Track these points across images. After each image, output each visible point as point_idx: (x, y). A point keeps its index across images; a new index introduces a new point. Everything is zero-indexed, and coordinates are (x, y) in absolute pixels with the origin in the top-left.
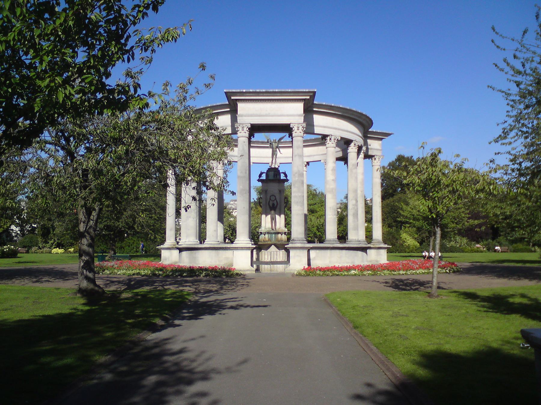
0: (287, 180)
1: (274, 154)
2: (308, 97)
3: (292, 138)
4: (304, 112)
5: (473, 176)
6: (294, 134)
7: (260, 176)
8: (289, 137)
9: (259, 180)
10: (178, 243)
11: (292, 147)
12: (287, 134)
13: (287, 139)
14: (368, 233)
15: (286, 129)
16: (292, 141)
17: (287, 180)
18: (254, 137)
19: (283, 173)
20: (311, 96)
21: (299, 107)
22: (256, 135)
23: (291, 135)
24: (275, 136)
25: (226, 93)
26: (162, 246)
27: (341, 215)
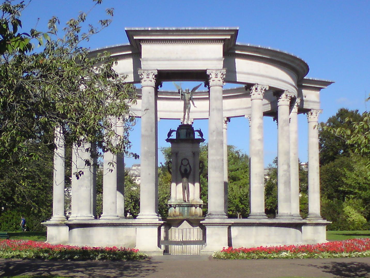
0: (203, 140)
1: (186, 107)
3: (209, 88)
7: (169, 135)
9: (168, 140)
12: (203, 83)
13: (203, 88)
15: (202, 76)
17: (203, 140)
20: (232, 36)
22: (164, 84)
23: (207, 84)
24: (187, 85)
26: (48, 222)
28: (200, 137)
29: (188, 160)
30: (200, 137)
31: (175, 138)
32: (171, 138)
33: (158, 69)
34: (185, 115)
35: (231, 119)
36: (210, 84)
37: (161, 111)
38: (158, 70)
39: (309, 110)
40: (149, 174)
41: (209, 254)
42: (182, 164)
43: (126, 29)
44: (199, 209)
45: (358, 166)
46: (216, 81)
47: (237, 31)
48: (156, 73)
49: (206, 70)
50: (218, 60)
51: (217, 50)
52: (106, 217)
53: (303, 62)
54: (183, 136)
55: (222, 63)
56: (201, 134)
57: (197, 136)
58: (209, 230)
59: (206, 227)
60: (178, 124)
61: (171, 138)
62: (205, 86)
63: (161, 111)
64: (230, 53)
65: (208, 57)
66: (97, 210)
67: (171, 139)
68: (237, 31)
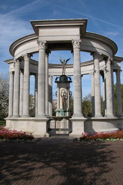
0: (71, 82)
6: (74, 50)
7: (56, 79)
9: (55, 82)
18: (50, 53)
20: (84, 23)
34: (63, 71)
35: (83, 75)
40: (42, 94)
41: (75, 137)
43: (31, 21)
44: (38, 59)
45: (34, 159)
46: (76, 47)
49: (71, 41)
50: (77, 35)
51: (76, 31)
54: (62, 80)
56: (71, 79)
57: (69, 80)
58: (74, 123)
59: (72, 122)
62: (72, 53)
64: (83, 35)
65: (72, 34)
68: (87, 20)
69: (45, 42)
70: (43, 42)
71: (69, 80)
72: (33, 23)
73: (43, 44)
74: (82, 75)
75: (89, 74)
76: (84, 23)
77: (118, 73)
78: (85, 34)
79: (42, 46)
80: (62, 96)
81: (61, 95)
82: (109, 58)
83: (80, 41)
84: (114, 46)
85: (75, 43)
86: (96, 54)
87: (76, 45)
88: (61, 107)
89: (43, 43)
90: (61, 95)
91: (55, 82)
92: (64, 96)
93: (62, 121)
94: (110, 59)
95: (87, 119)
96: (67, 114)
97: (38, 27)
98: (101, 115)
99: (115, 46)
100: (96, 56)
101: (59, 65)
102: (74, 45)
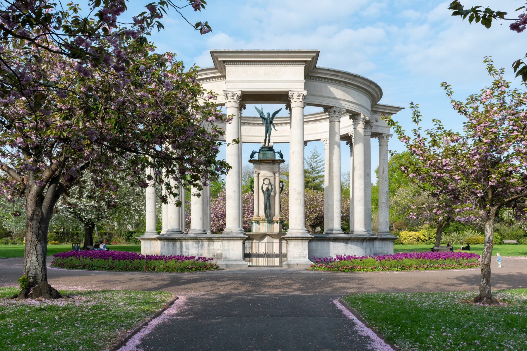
0: (283, 161)
1: (268, 131)
2: (310, 59)
3: (290, 110)
4: (305, 78)
5: (511, 169)
6: (293, 104)
7: (252, 156)
8: (286, 109)
9: (250, 161)
10: (419, 136)
11: (290, 123)
12: (283, 106)
13: (284, 112)
14: (311, 192)
15: (282, 97)
16: (290, 117)
17: (283, 161)
18: (245, 109)
19: (278, 153)
20: (313, 59)
21: (299, 71)
22: (248, 106)
23: (289, 106)
24: (269, 108)
25: (212, 53)
26: (141, 237)
27: (276, 170)
28: (280, 159)
29: (269, 179)
30: (280, 159)
31: (257, 159)
32: (253, 159)
33: (243, 90)
35: (308, 143)
36: (292, 106)
37: (244, 136)
38: (242, 91)
39: (381, 134)
42: (264, 183)
46: (296, 103)
47: (318, 53)
48: (240, 94)
49: (288, 92)
52: (290, 233)
53: (377, 86)
55: (303, 84)
56: (282, 156)
60: (259, 146)
61: (253, 159)
63: (244, 136)
64: (312, 73)
65: (290, 78)
66: (289, 136)
67: (254, 160)
69: (240, 94)
70: (235, 93)
71: (277, 157)
72: (215, 55)
73: (235, 98)
74: (305, 143)
75: (320, 140)
76: (313, 58)
77: (383, 142)
78: (316, 73)
79: (233, 100)
80: (263, 192)
81: (262, 188)
82: (362, 116)
83: (305, 93)
84: (374, 90)
85: (295, 95)
86: (335, 111)
87: (297, 100)
88: (262, 213)
89: (234, 95)
90: (262, 188)
91: (250, 161)
92: (268, 189)
93: (265, 240)
94: (364, 119)
95: (313, 237)
96: (276, 228)
97: (224, 62)
98: (305, 229)
99: (377, 90)
100: (334, 116)
101: (254, 118)
102: (292, 101)
